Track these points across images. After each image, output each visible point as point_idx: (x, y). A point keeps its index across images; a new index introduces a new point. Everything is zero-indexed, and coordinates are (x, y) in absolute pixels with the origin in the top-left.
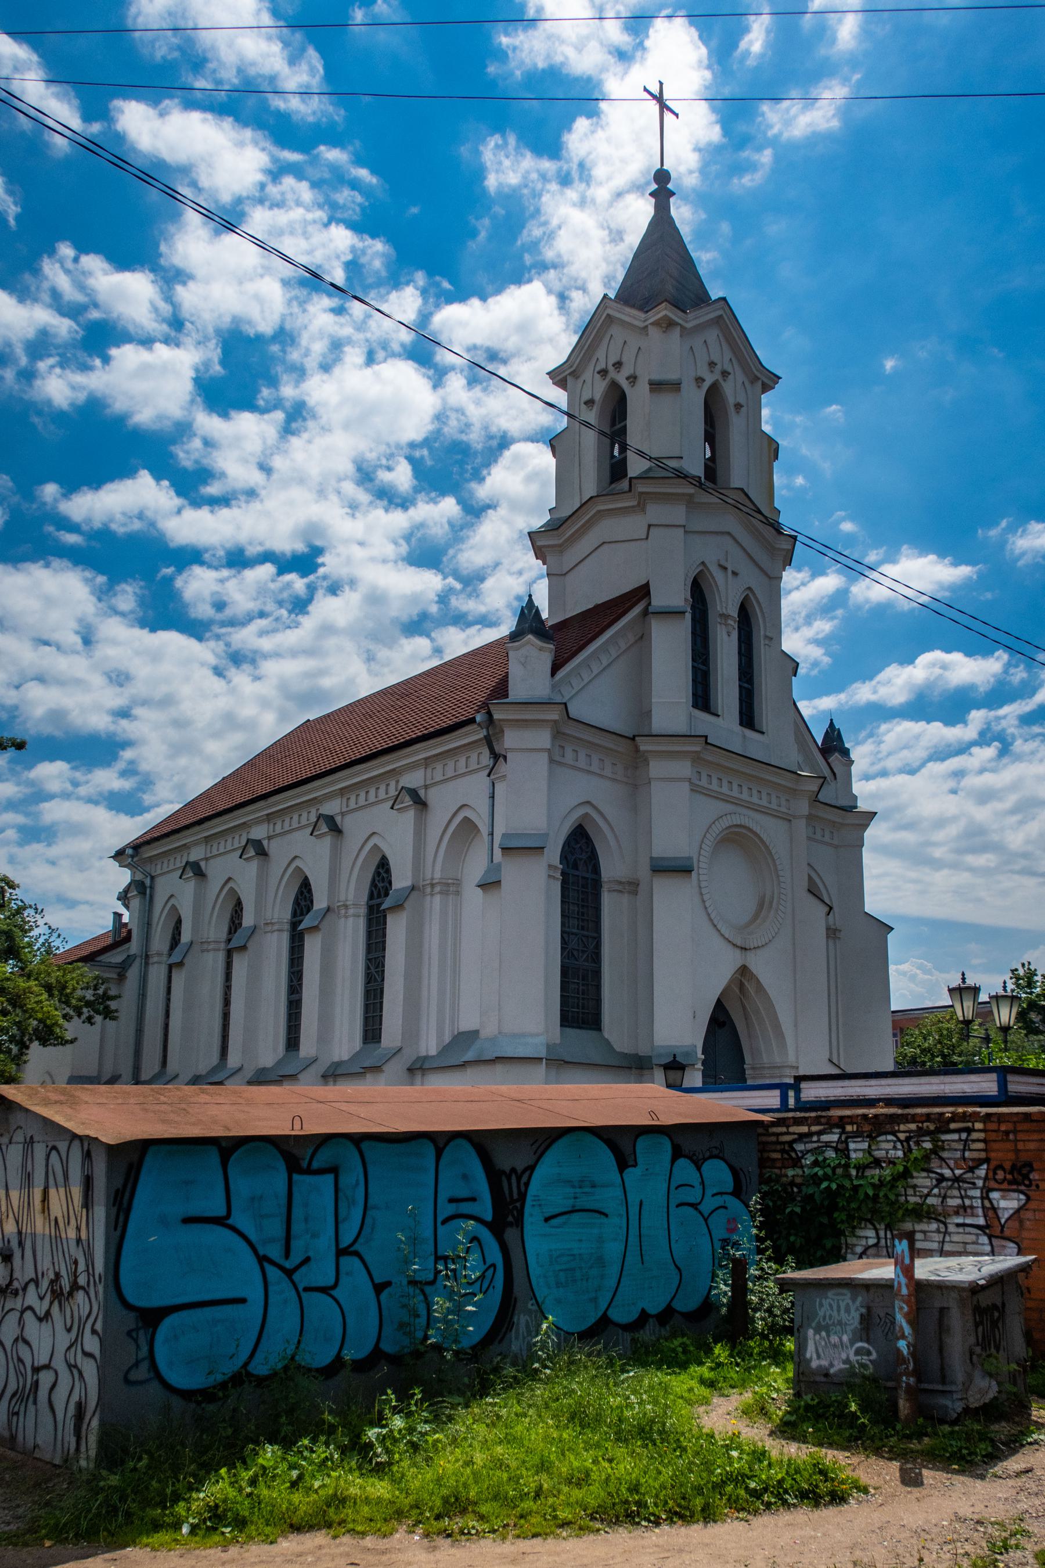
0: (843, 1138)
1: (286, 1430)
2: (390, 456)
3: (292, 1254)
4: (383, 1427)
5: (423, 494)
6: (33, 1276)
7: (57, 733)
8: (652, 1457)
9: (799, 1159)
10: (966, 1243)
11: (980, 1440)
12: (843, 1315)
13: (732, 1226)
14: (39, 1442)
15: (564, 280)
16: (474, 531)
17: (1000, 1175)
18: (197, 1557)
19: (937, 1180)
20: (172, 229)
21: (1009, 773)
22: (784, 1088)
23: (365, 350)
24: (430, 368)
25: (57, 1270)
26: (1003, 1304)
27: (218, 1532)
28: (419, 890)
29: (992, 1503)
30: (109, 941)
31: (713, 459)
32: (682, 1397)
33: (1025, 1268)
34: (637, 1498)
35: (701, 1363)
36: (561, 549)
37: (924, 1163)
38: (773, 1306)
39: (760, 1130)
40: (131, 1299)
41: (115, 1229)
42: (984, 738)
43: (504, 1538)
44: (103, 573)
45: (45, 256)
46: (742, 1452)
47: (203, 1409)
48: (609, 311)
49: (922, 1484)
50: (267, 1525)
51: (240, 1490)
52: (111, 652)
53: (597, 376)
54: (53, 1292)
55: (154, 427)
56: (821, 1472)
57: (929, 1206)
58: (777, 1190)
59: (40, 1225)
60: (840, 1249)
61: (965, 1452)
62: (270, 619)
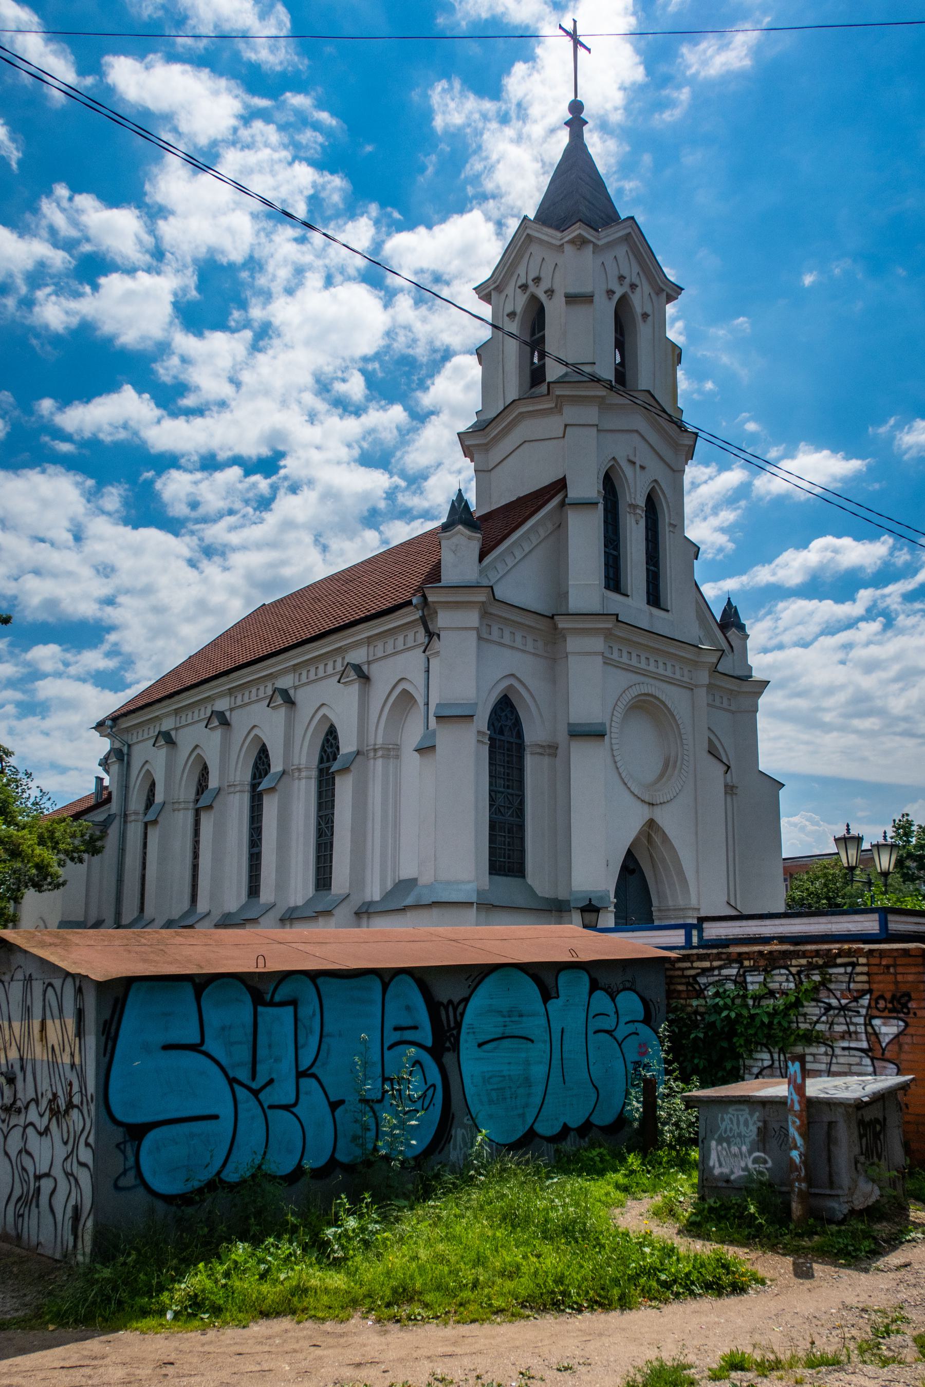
0: (741, 972)
1: (255, 1229)
2: (345, 369)
3: (258, 1076)
4: (339, 1226)
5: (374, 402)
6: (34, 1096)
7: (51, 620)
8: (575, 1253)
9: (702, 991)
10: (851, 1065)
11: (865, 1238)
12: (742, 1128)
13: (643, 1050)
14: (42, 1240)
15: (502, 209)
16: (419, 435)
17: (882, 1004)
18: (180, 1339)
19: (825, 1009)
20: (155, 170)
21: (893, 645)
22: (688, 928)
23: (324, 275)
24: (381, 289)
25: (54, 1091)
26: (885, 1119)
27: (198, 1318)
28: (364, 754)
29: (875, 1293)
30: (92, 802)
31: (622, 364)
32: (600, 1201)
33: (904, 1087)
34: (562, 1288)
35: (616, 1171)
36: (486, 448)
37: (813, 994)
38: (680, 1120)
39: (667, 966)
40: (119, 1116)
41: (105, 1055)
42: (870, 614)
43: (446, 1324)
44: (92, 477)
45: (43, 197)
46: (654, 1248)
47: (183, 1211)
48: (529, 231)
49: (813, 1276)
50: (240, 1312)
51: (216, 1281)
52: (99, 547)
53: (518, 291)
54: (51, 1110)
55: (140, 347)
56: (724, 1266)
57: (818, 1031)
58: (682, 1018)
59: (39, 1052)
60: (738, 1070)
61: (851, 1248)
62: (238, 516)
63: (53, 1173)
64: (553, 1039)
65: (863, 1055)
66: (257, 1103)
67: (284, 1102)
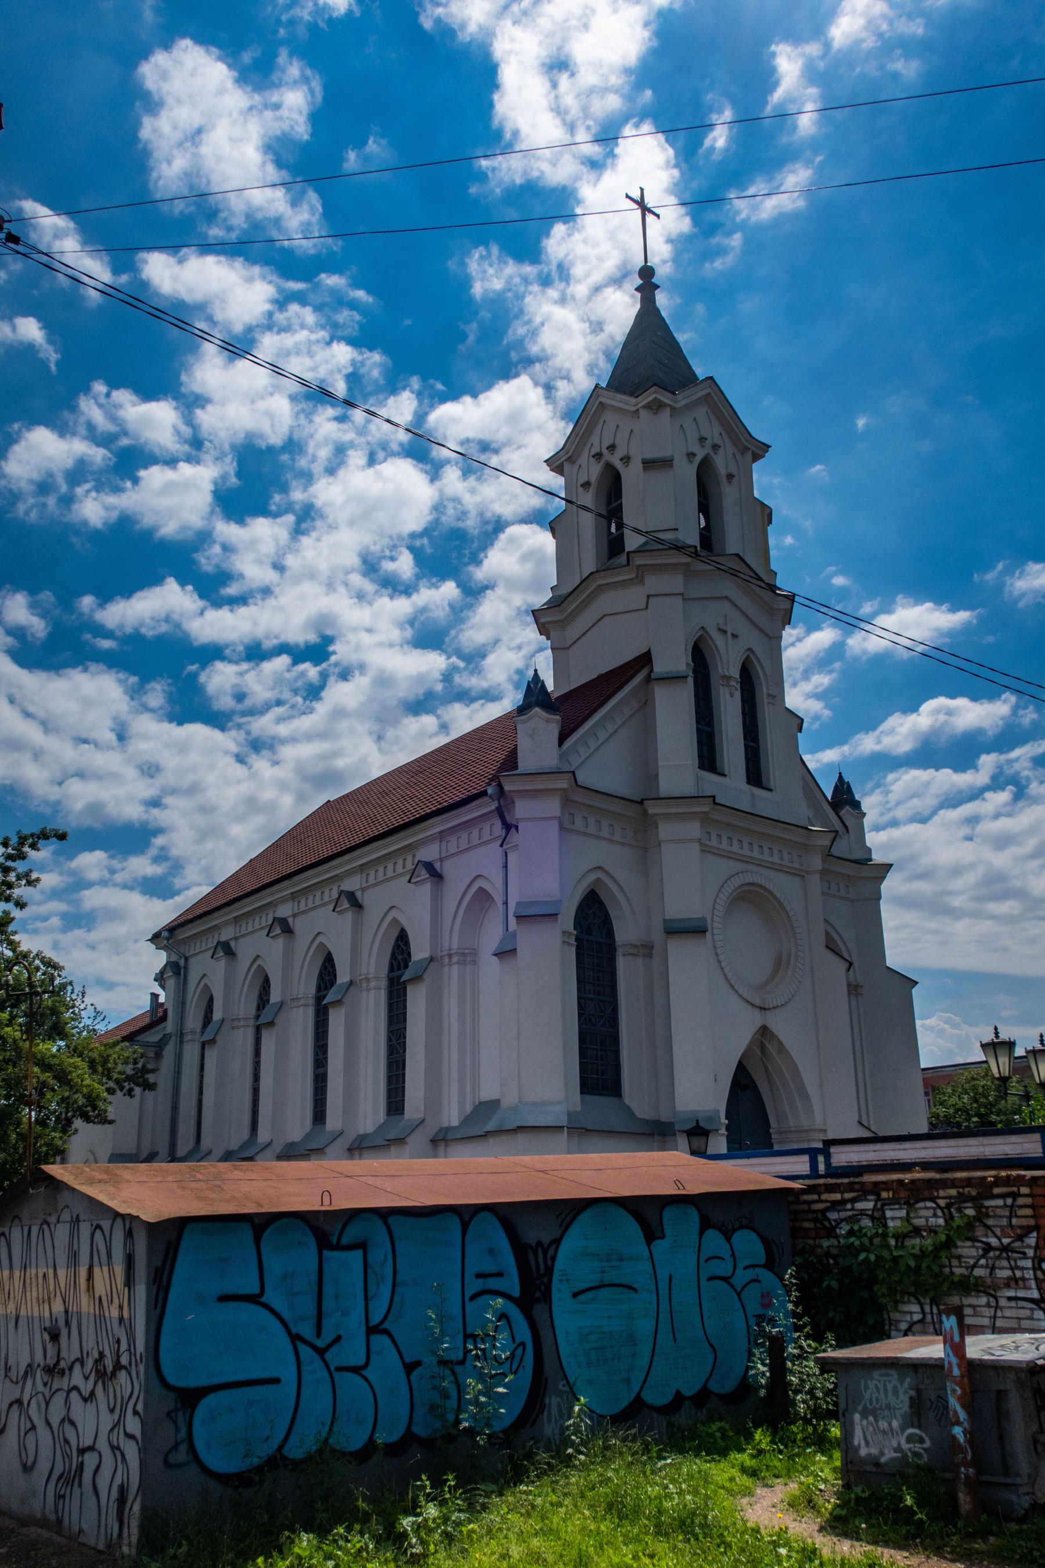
2: (394, 547)
3: (324, 1332)
6: (79, 1356)
7: (96, 825)
8: (695, 1554)
9: (833, 1228)
10: (1020, 1319)
13: (766, 1301)
14: (85, 1527)
15: (549, 371)
16: (474, 611)
19: (983, 1249)
21: (1026, 817)
22: (813, 1154)
30: (147, 1021)
31: (708, 528)
32: (723, 1487)
35: (741, 1450)
36: (563, 624)
39: (791, 1199)
40: (171, 1380)
41: (156, 1308)
42: (997, 783)
44: (135, 674)
46: (791, 1549)
48: (601, 399)
52: (143, 746)
53: (593, 460)
54: (97, 1371)
57: (976, 1278)
59: (85, 1305)
61: (1036, 1554)
62: (287, 706)
63: (98, 1446)
64: (660, 1287)
65: (1034, 1306)
66: (323, 1365)
67: (353, 1363)
